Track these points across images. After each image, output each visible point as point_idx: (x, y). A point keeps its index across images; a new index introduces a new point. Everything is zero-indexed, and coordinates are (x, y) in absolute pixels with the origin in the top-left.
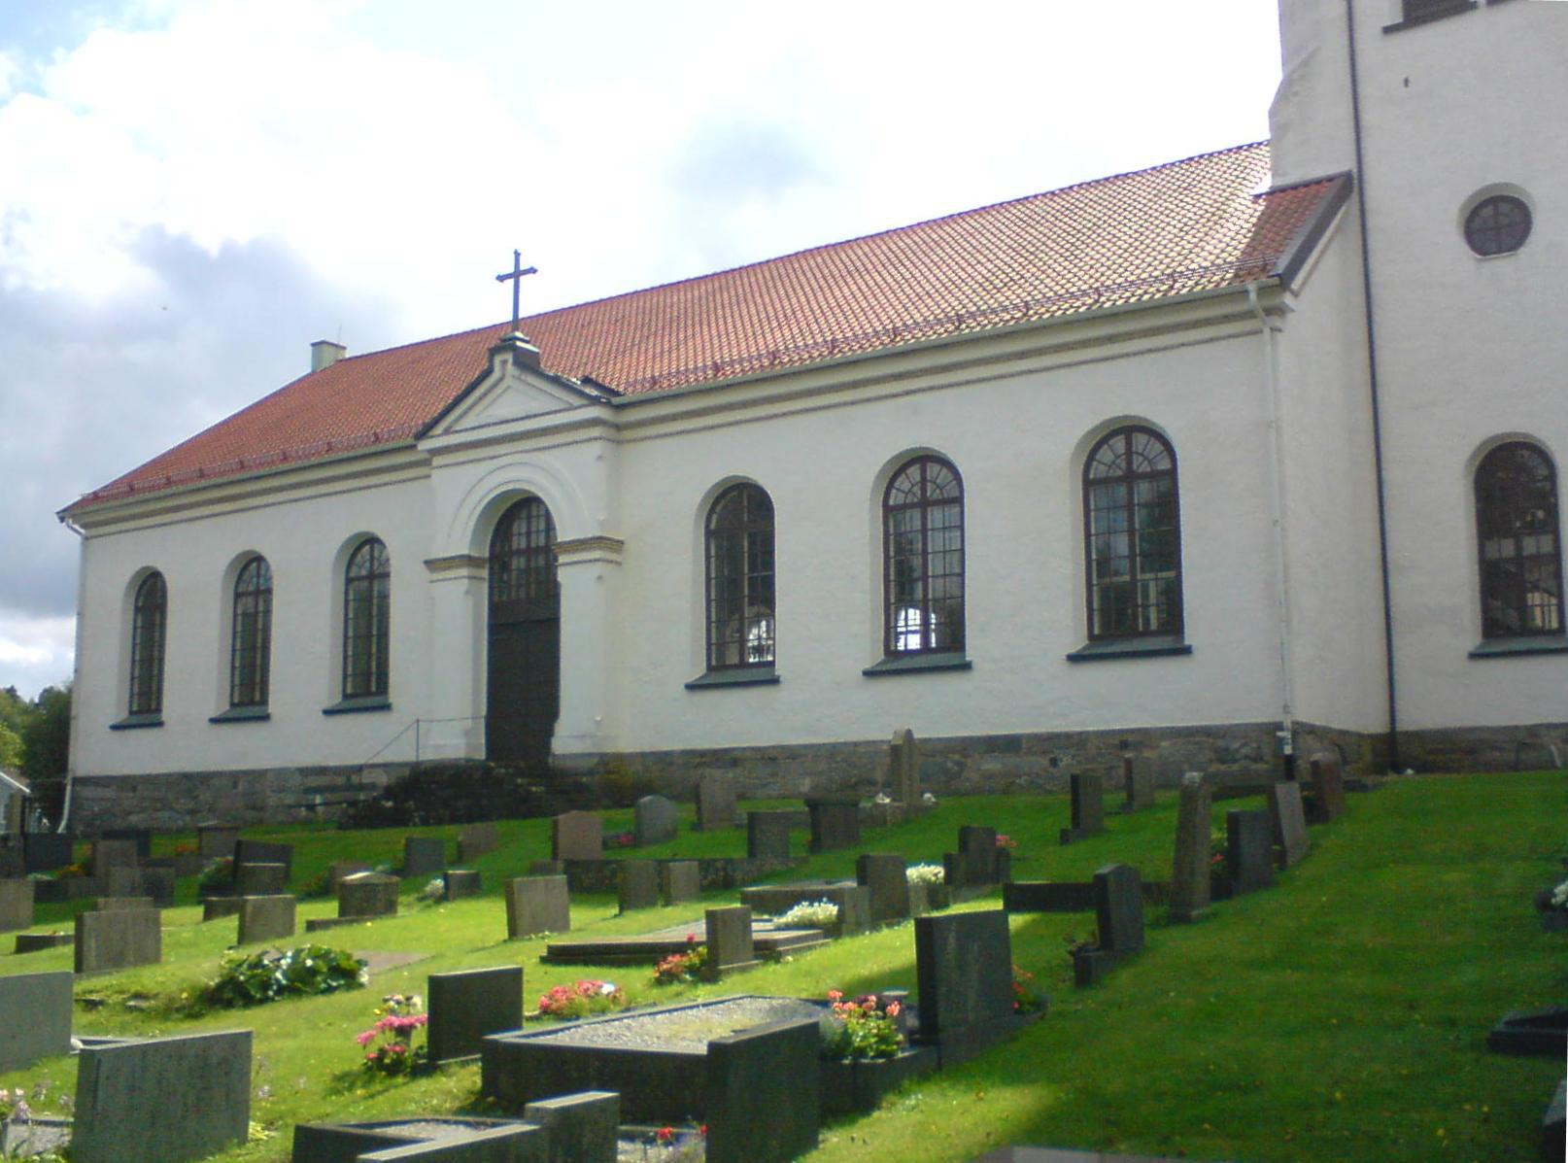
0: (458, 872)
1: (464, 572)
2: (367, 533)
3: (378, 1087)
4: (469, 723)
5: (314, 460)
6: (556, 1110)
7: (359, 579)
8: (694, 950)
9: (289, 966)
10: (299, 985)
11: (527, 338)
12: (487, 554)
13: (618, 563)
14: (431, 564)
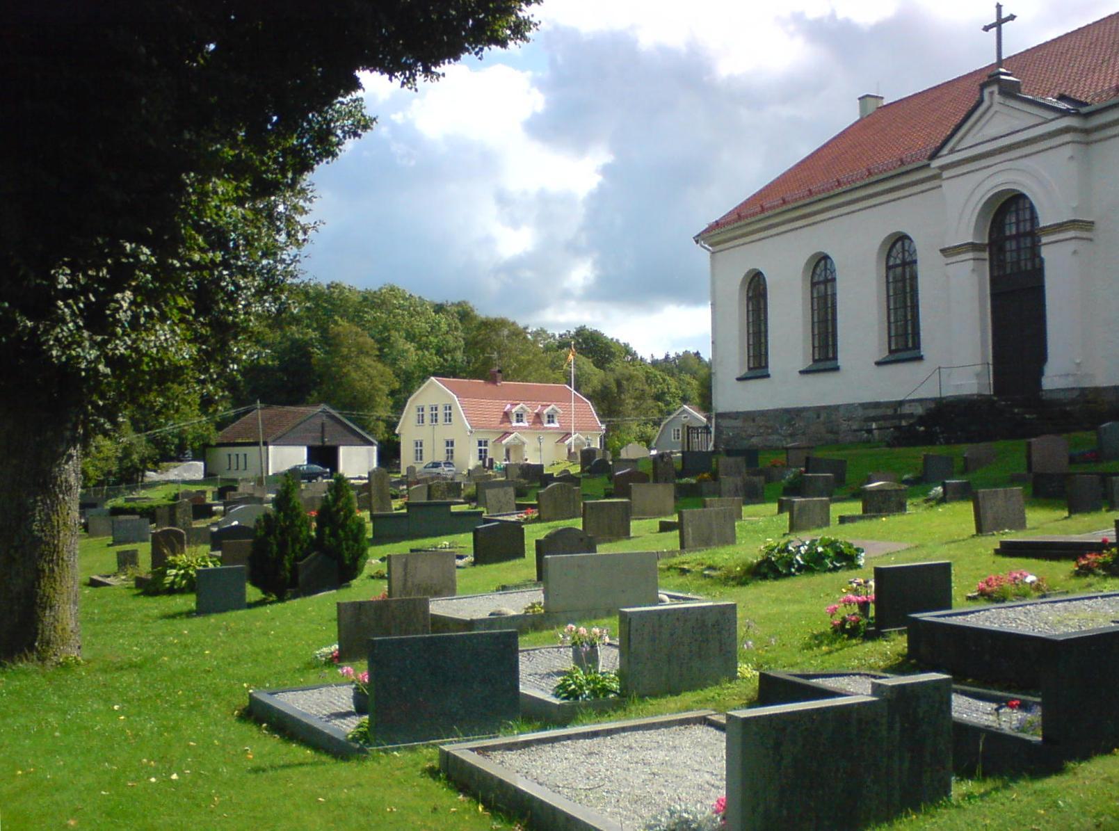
0: (954, 481)
1: (970, 255)
2: (899, 232)
3: (837, 646)
4: (978, 368)
5: (858, 184)
6: (893, 687)
7: (896, 266)
8: (1108, 550)
9: (806, 551)
10: (812, 565)
11: (1009, 72)
12: (986, 241)
13: (1091, 240)
14: (945, 252)
